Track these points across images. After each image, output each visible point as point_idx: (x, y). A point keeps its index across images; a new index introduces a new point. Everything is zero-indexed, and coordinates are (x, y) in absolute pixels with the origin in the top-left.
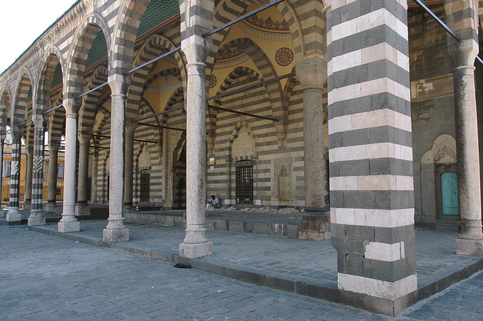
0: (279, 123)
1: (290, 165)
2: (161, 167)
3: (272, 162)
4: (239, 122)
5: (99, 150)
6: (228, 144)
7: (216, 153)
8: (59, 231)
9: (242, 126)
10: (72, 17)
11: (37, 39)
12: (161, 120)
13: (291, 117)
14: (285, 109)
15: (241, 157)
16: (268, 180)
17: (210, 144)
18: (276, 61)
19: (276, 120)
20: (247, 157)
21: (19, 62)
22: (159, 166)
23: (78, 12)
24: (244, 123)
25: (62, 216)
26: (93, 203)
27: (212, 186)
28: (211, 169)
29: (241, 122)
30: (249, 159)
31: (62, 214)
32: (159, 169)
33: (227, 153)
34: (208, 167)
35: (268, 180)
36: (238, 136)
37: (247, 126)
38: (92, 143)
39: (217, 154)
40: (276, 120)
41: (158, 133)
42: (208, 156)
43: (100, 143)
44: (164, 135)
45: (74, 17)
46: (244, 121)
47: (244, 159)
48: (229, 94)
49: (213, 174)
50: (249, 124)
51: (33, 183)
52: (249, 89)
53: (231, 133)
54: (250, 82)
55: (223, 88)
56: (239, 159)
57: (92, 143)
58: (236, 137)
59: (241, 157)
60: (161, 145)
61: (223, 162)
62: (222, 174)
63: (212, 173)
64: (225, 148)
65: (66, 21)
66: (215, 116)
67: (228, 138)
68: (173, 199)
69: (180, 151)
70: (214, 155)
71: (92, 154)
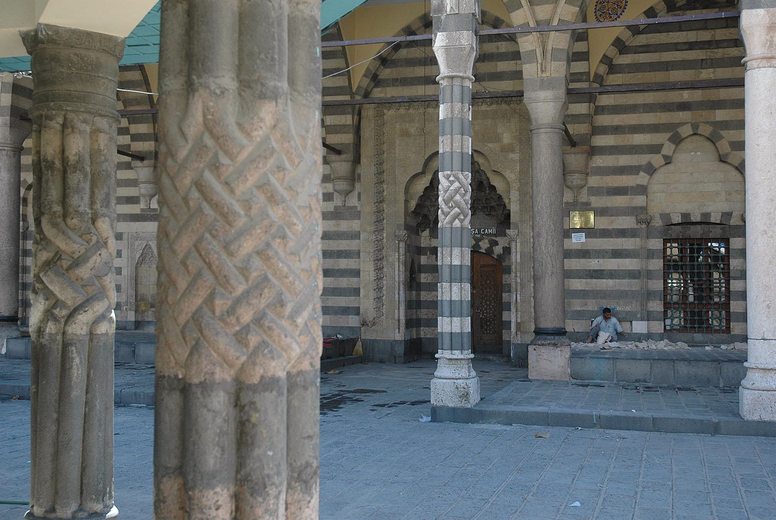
0: (576, 149)
3: (125, 236)
4: (687, 123)
12: (359, 87)
13: (600, 141)
19: (140, 157)
25: (437, 359)
27: (577, 284)
28: (574, 240)
30: (713, 220)
31: (436, 356)
32: (336, 229)
34: (567, 233)
36: (673, 160)
40: (140, 157)
41: (152, 134)
44: (367, 132)
48: (646, 49)
49: (584, 254)
50: (724, 133)
52: (725, 44)
53: (655, 149)
54: (727, 27)
55: (635, 30)
56: (677, 219)
58: (668, 161)
59: (685, 215)
60: (357, 160)
64: (632, 187)
68: (406, 316)
69: (423, 183)
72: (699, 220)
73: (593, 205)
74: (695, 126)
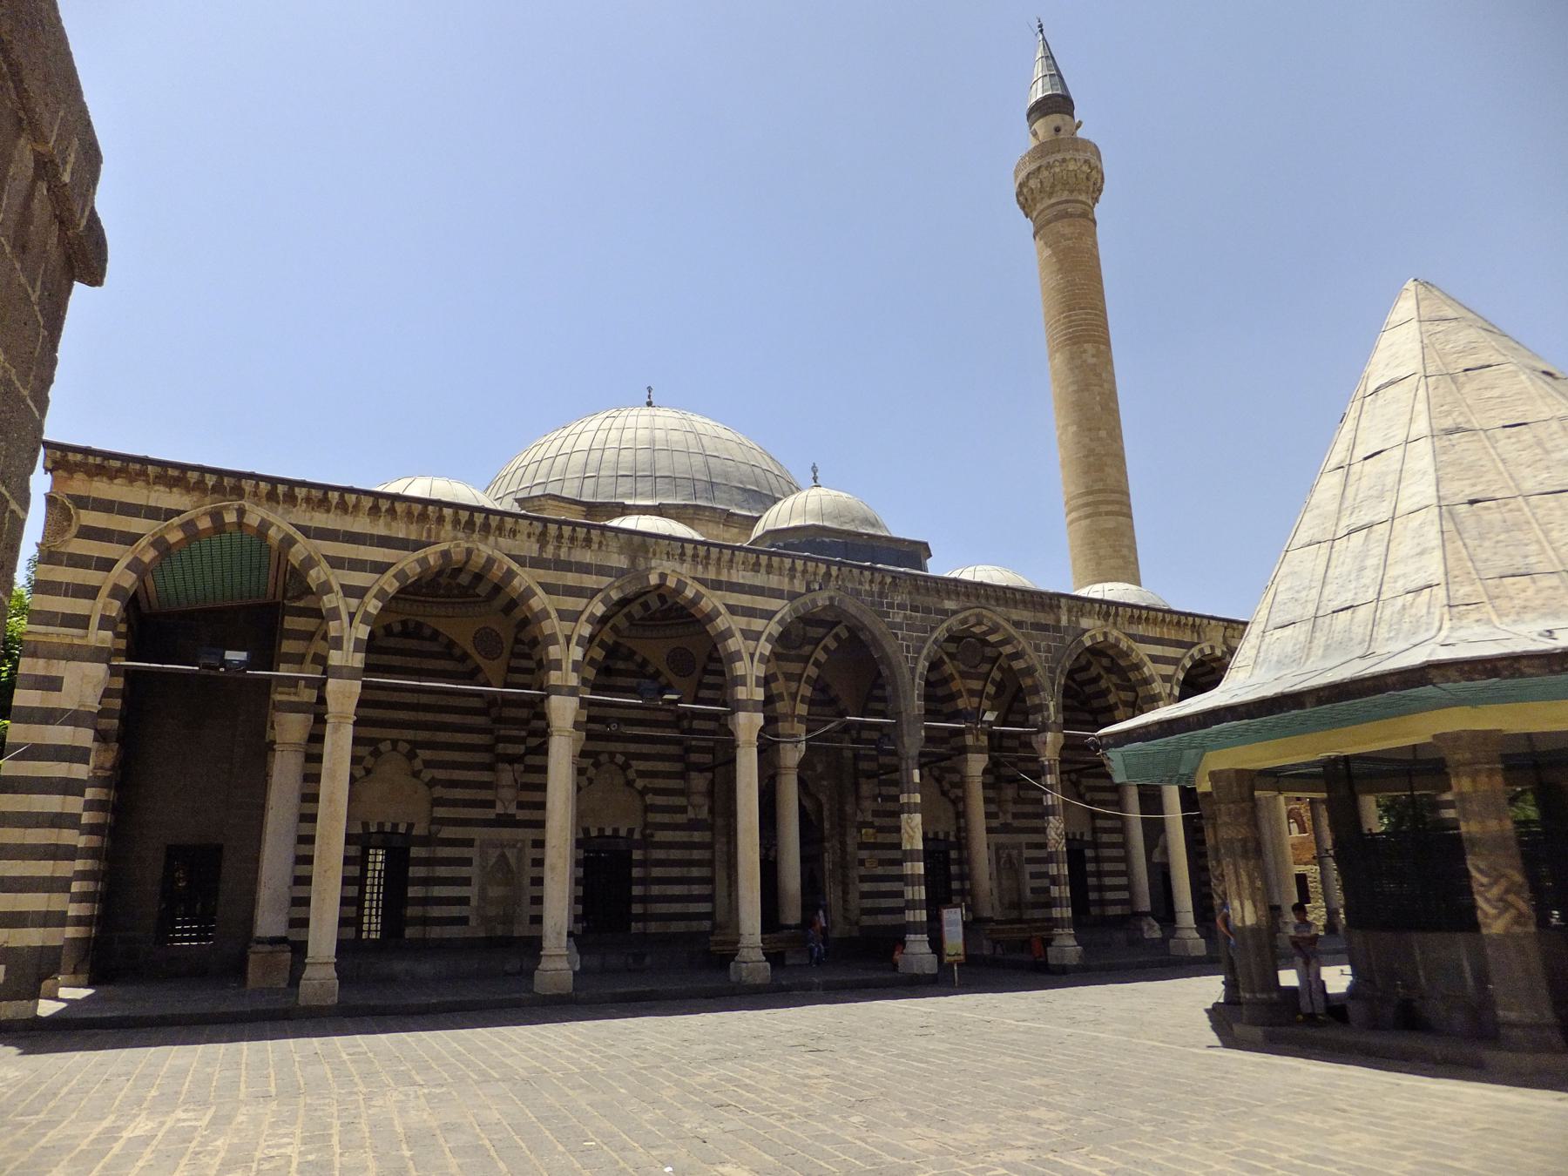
1: (1020, 854)
3: (477, 843)
16: (466, 882)
35: (466, 882)
37: (411, 756)
50: (634, 763)
74: (395, 743)
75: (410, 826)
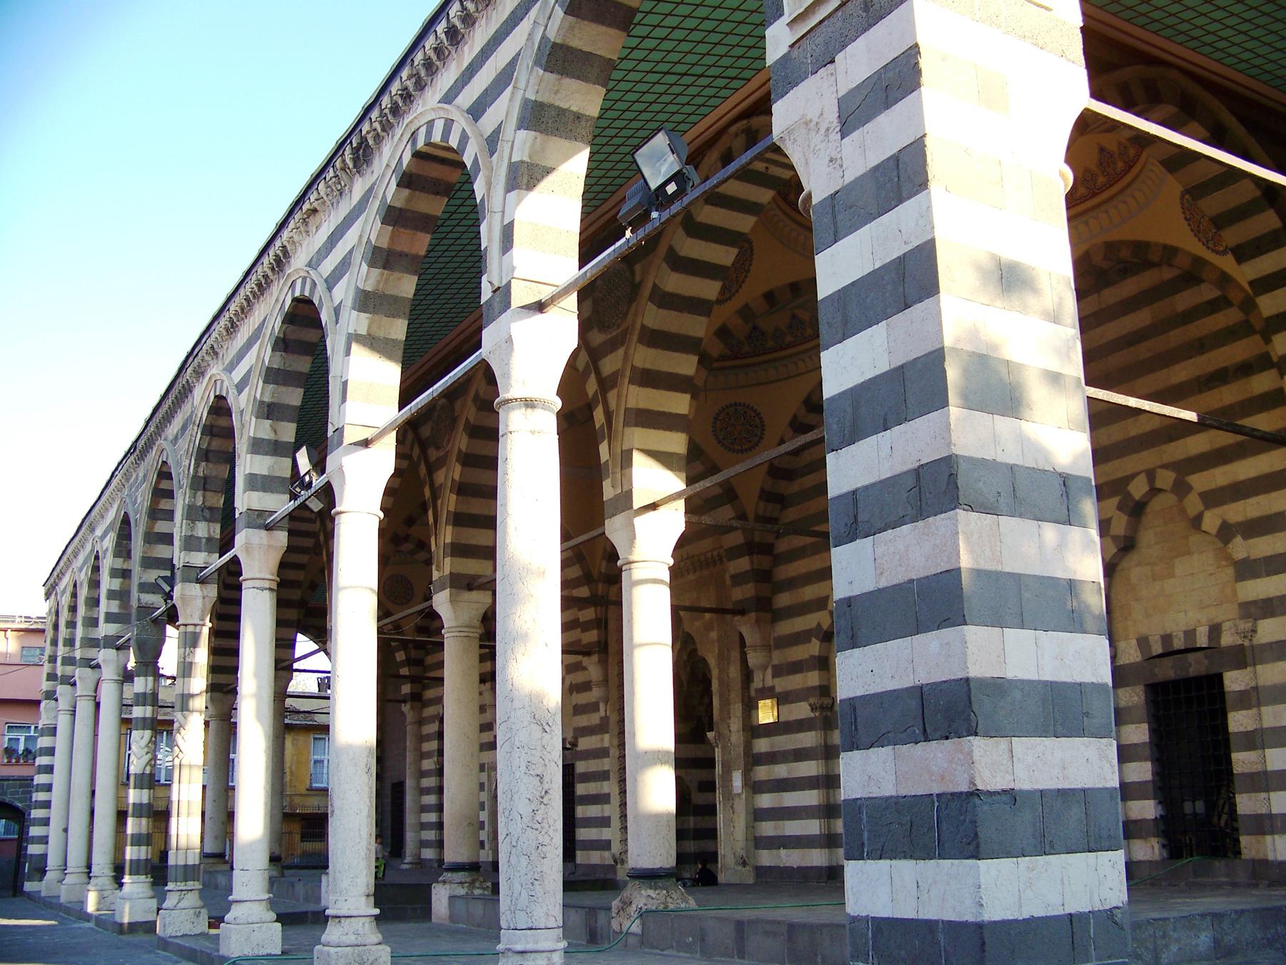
0: (746, 617)
2: (607, 737)
5: (425, 688)
6: (814, 647)
7: (777, 680)
8: (221, 953)
9: (1154, 491)
10: (259, 285)
11: (188, 357)
14: (763, 576)
15: (1167, 639)
17: (754, 647)
18: (758, 414)
20: (1190, 634)
21: (152, 428)
22: (599, 737)
23: (273, 269)
24: (1166, 479)
26: (408, 866)
27: (766, 801)
29: (1151, 475)
33: (813, 678)
37: (1181, 488)
38: (402, 664)
39: (782, 684)
42: (753, 693)
43: (776, 551)
45: (262, 288)
46: (1164, 466)
47: (1178, 644)
51: (129, 830)
56: (1157, 649)
57: (402, 664)
61: (802, 710)
62: (799, 755)
63: (766, 753)
65: (247, 299)
66: (767, 549)
67: (814, 625)
70: (772, 688)
71: (742, 612)
72: (1160, 651)
73: (778, 690)
75: (1215, 630)
